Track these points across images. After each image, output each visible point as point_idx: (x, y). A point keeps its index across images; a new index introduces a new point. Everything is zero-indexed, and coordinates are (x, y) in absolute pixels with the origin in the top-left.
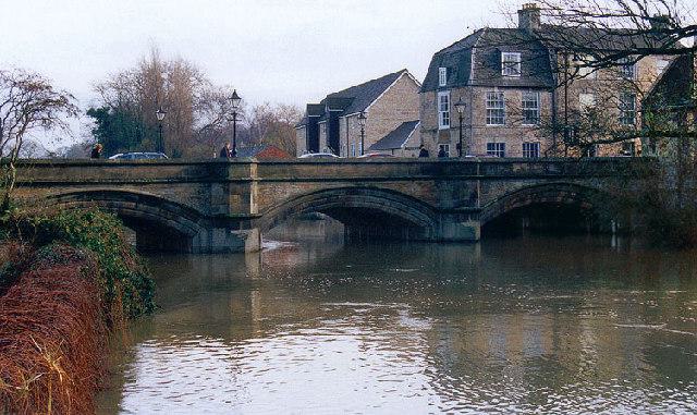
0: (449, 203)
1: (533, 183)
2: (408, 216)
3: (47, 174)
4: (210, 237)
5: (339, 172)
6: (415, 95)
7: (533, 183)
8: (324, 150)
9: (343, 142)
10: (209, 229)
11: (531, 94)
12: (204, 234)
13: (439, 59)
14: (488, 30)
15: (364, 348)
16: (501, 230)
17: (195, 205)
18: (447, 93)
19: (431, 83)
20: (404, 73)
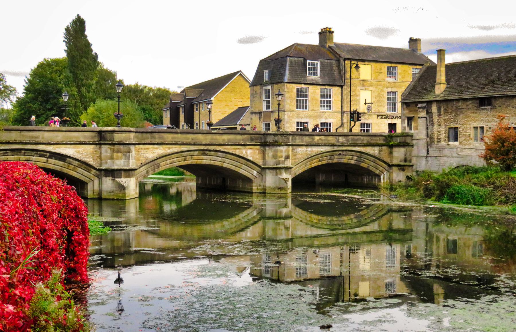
0: (271, 163)
1: (327, 149)
2: (241, 171)
3: (155, 138)
4: (100, 184)
5: (193, 139)
6: (247, 89)
7: (327, 149)
8: (183, 126)
9: (196, 120)
10: (99, 177)
11: (471, 322)
12: (96, 182)
13: (264, 64)
14: (298, 45)
15: (210, 261)
16: (441, 61)
17: (89, 160)
18: (269, 87)
19: (258, 81)
20: (239, 73)
